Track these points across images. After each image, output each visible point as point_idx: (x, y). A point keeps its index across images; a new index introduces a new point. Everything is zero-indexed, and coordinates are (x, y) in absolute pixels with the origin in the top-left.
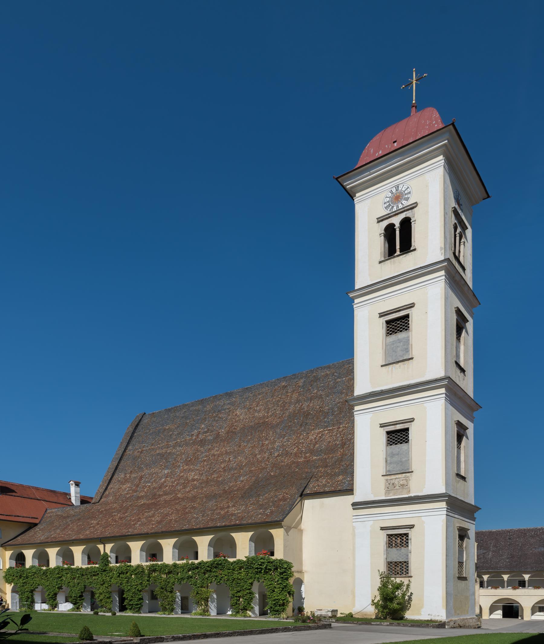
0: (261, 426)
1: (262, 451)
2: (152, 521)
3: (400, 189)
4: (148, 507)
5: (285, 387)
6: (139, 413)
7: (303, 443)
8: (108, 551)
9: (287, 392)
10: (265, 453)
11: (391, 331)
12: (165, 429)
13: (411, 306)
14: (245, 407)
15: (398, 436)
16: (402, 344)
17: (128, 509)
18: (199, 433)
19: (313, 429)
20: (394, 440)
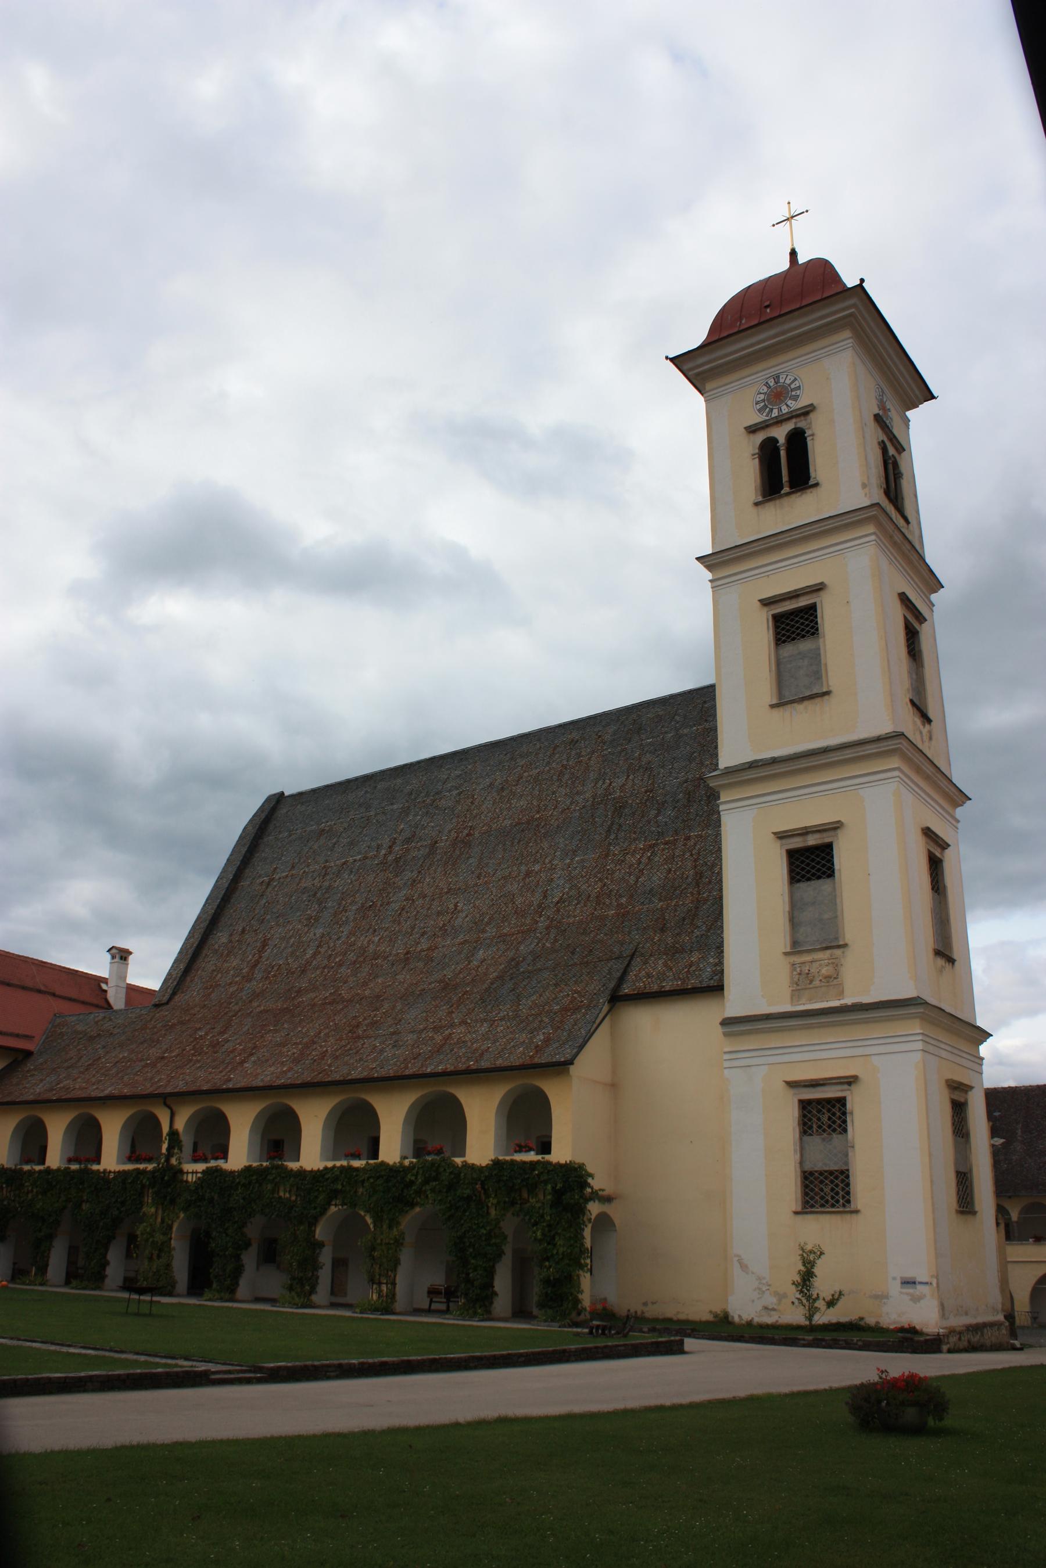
3: (782, 381)
8: (180, 1125)
9: (579, 755)
11: (784, 635)
13: (819, 588)
15: (811, 861)
19: (635, 839)
20: (803, 869)
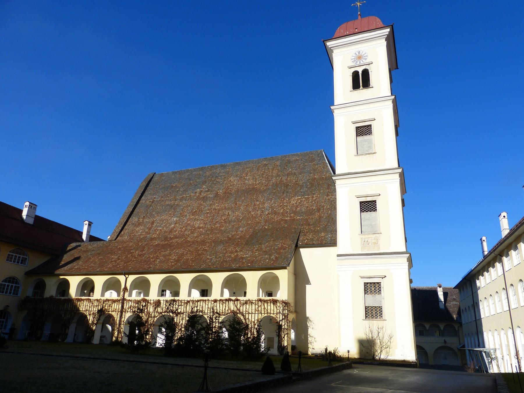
0: (252, 191)
1: (254, 209)
2: (169, 259)
4: (164, 247)
5: (266, 165)
6: (151, 173)
7: (287, 206)
10: (258, 211)
12: (172, 186)
14: (237, 176)
16: (367, 143)
17: (144, 247)
18: (201, 192)
